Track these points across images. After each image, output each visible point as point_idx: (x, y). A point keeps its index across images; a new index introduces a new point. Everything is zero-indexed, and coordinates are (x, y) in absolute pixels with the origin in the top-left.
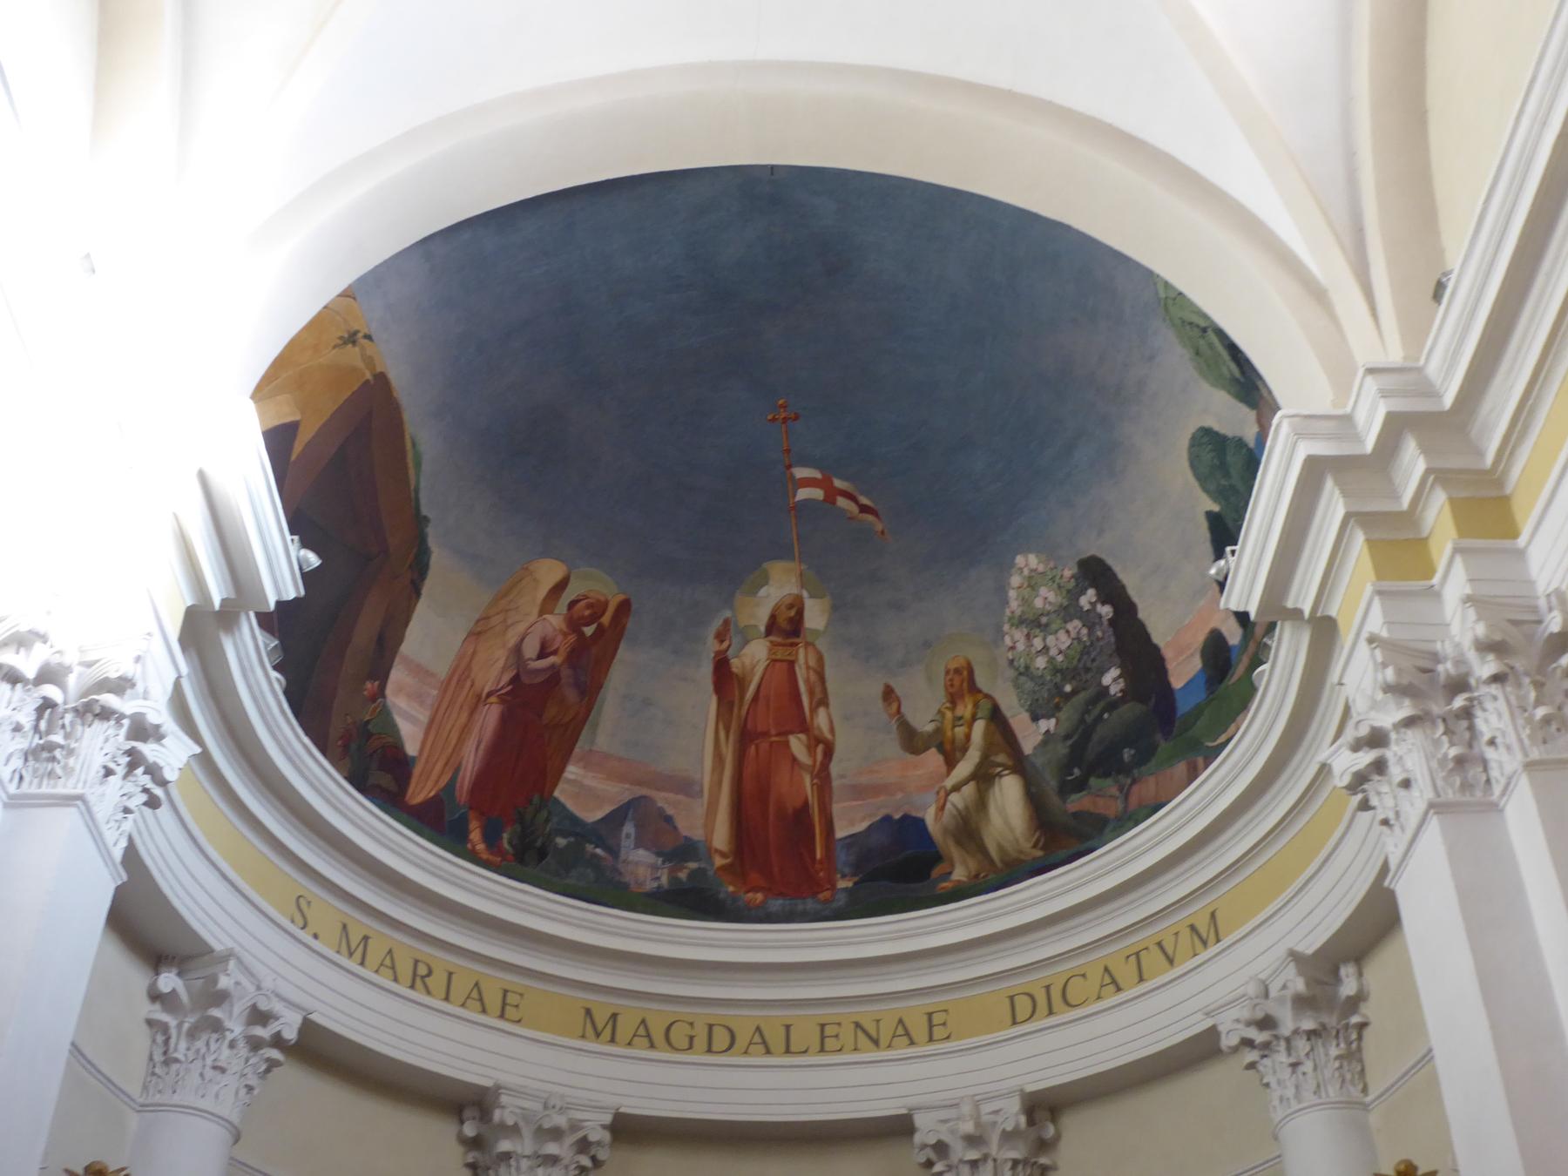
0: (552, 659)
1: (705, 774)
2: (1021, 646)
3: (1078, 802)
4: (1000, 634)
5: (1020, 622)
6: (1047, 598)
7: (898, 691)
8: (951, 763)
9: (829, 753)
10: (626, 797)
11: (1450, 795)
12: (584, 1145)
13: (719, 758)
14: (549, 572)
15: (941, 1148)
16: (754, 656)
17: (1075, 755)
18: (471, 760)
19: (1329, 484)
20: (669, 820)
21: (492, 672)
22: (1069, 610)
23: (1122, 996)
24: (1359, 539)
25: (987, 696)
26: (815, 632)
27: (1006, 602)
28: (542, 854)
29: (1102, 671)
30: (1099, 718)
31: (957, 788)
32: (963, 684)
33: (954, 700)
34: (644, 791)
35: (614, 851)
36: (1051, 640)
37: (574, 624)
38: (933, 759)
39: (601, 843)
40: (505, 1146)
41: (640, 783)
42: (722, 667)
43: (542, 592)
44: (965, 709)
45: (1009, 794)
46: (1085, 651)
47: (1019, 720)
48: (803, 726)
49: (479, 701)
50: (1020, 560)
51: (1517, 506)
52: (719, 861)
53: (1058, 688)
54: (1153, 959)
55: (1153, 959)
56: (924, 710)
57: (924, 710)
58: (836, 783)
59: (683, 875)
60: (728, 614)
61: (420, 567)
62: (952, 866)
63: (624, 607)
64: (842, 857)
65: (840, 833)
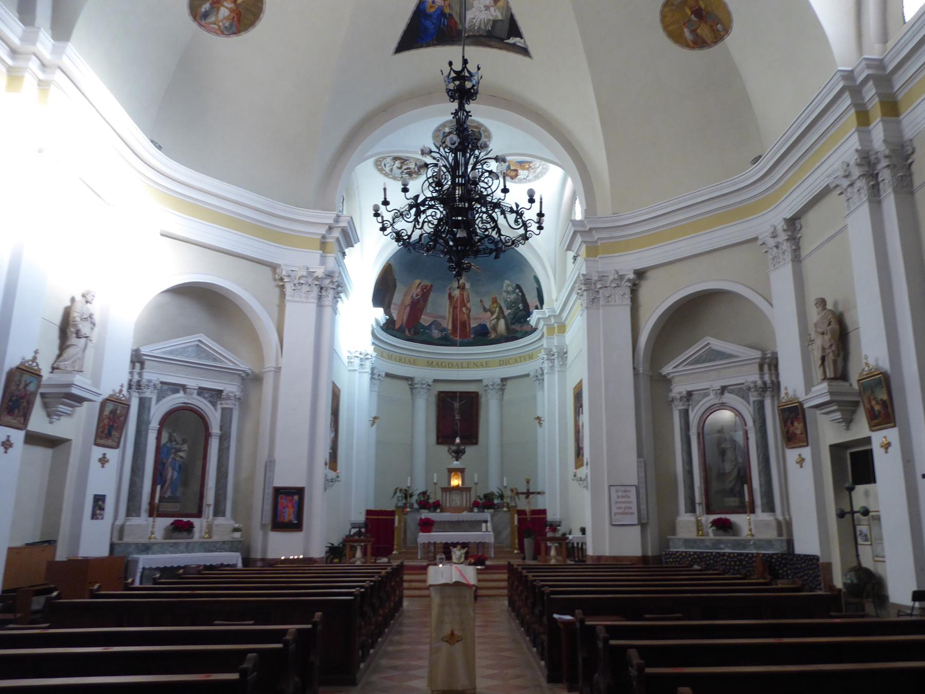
0: (418, 297)
1: (447, 315)
2: (505, 296)
3: (514, 327)
4: (502, 294)
5: (505, 292)
6: (510, 289)
7: (483, 300)
8: (492, 315)
9: (470, 311)
10: (432, 320)
11: (549, 371)
12: (429, 385)
13: (449, 312)
14: (418, 282)
15: (487, 386)
16: (457, 293)
17: (514, 317)
18: (405, 318)
19: (579, 235)
20: (440, 324)
21: (408, 301)
22: (514, 292)
23: (518, 364)
24: (584, 246)
25: (499, 304)
26: (468, 289)
27: (503, 288)
28: (418, 333)
29: (520, 304)
30: (518, 313)
31: (493, 320)
32: (495, 301)
33: (493, 303)
34: (435, 319)
35: (431, 331)
36: (511, 296)
37: (422, 290)
38: (489, 314)
39: (428, 330)
40: (416, 386)
41: (435, 317)
42: (450, 295)
43: (416, 285)
44: (495, 305)
45: (502, 323)
46: (517, 300)
47: (505, 309)
48: (465, 306)
49: (406, 307)
50: (506, 281)
51: (567, 327)
52: (450, 332)
53: (511, 305)
54: (522, 359)
55: (522, 359)
56: (488, 304)
57: (488, 304)
58: (471, 317)
59: (443, 334)
60: (451, 285)
61: (395, 286)
62: (491, 334)
63: (431, 285)
64: (472, 331)
65: (472, 327)
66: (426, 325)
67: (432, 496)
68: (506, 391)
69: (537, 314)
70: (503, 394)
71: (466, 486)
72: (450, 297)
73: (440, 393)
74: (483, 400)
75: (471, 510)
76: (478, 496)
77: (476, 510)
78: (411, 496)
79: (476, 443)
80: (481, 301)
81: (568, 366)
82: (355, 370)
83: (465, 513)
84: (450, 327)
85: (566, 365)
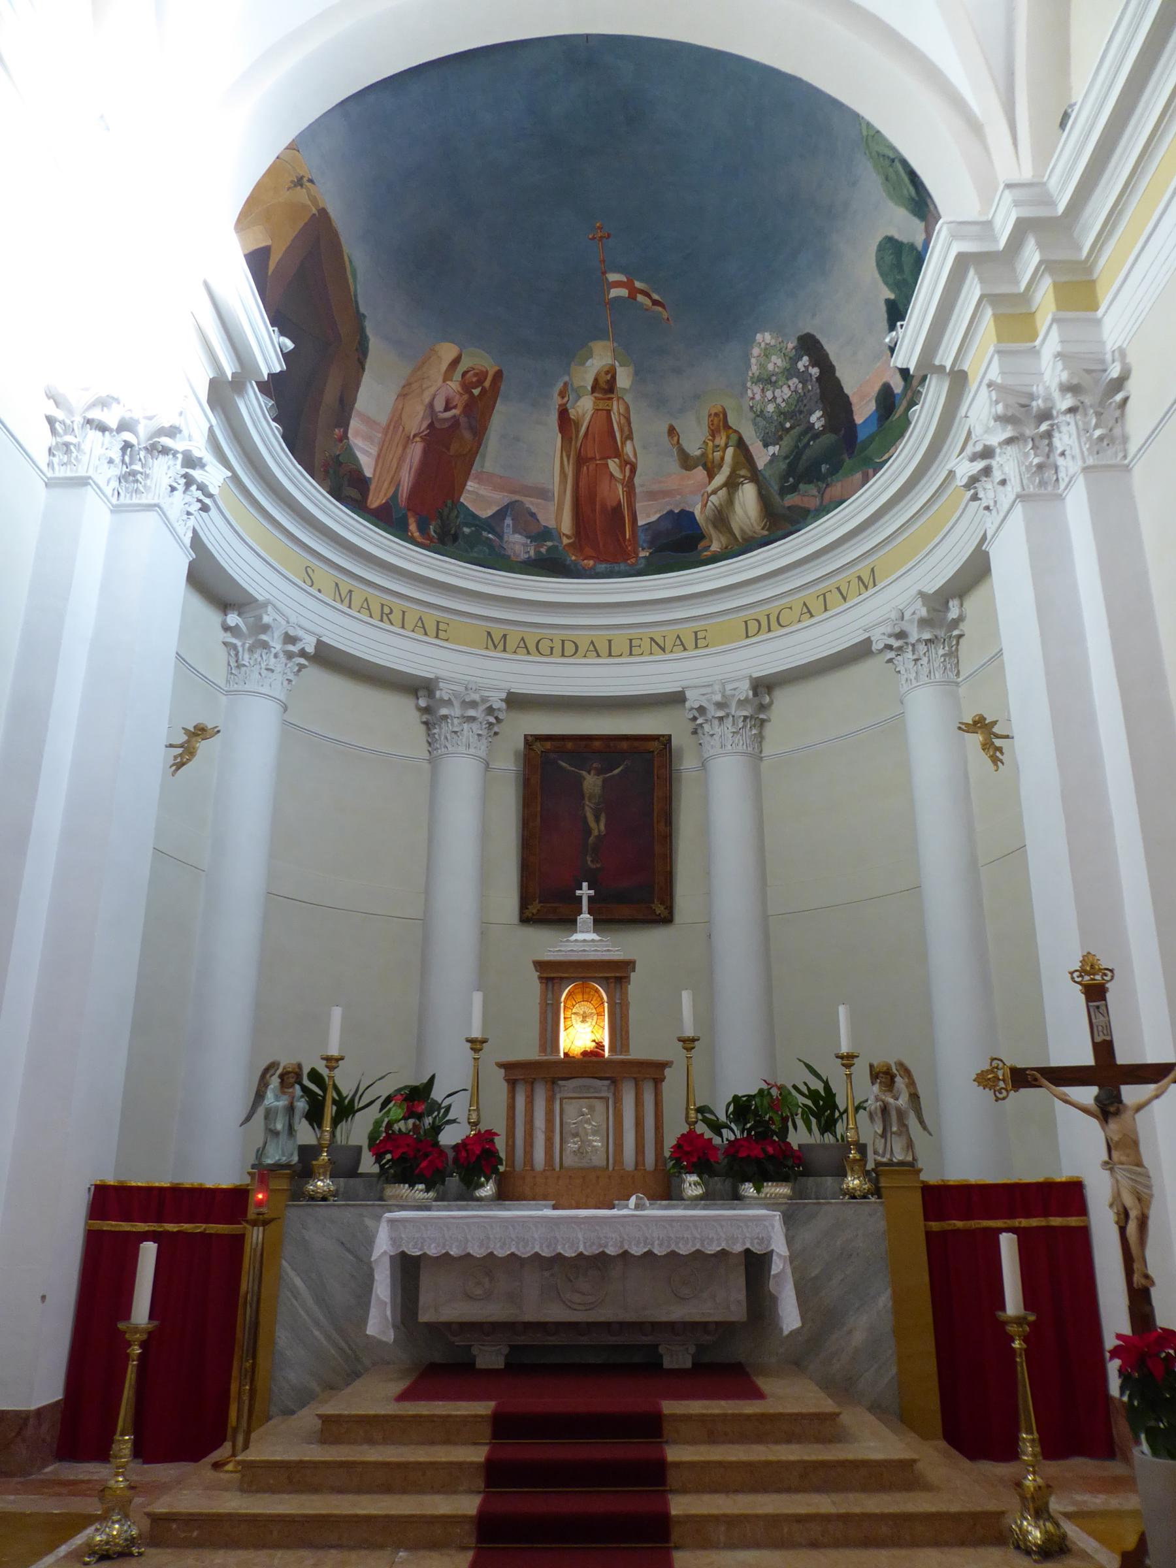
3: (791, 500)
5: (758, 380)
6: (776, 363)
8: (711, 476)
9: (633, 470)
12: (490, 710)
14: (448, 352)
15: (702, 710)
16: (585, 407)
17: (791, 470)
18: (406, 479)
21: (416, 422)
22: (790, 372)
24: (988, 313)
27: (749, 366)
29: (811, 413)
31: (714, 492)
32: (720, 424)
33: (713, 434)
35: (500, 536)
36: (778, 392)
37: (467, 387)
38: (700, 473)
39: (492, 531)
40: (444, 711)
41: (513, 492)
42: (563, 414)
43: (444, 366)
44: (721, 440)
45: (748, 494)
46: (800, 400)
49: (408, 440)
50: (759, 337)
52: (566, 541)
53: (782, 425)
56: (694, 440)
57: (694, 440)
60: (566, 378)
64: (642, 537)
65: (640, 523)
66: (485, 513)
67: (459, 1109)
68: (769, 730)
69: (954, 236)
70: (760, 738)
71: (638, 1051)
72: (565, 420)
73: (532, 741)
74: (687, 765)
75: (667, 1192)
76: (700, 1110)
77: (692, 1185)
78: (346, 1110)
79: (667, 919)
80: (672, 431)
81: (1133, 448)
82: (83, 482)
83: (628, 1209)
84: (566, 525)
85: (1125, 439)
